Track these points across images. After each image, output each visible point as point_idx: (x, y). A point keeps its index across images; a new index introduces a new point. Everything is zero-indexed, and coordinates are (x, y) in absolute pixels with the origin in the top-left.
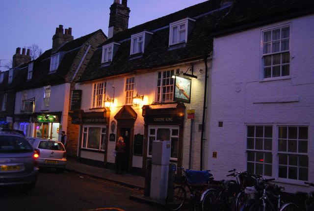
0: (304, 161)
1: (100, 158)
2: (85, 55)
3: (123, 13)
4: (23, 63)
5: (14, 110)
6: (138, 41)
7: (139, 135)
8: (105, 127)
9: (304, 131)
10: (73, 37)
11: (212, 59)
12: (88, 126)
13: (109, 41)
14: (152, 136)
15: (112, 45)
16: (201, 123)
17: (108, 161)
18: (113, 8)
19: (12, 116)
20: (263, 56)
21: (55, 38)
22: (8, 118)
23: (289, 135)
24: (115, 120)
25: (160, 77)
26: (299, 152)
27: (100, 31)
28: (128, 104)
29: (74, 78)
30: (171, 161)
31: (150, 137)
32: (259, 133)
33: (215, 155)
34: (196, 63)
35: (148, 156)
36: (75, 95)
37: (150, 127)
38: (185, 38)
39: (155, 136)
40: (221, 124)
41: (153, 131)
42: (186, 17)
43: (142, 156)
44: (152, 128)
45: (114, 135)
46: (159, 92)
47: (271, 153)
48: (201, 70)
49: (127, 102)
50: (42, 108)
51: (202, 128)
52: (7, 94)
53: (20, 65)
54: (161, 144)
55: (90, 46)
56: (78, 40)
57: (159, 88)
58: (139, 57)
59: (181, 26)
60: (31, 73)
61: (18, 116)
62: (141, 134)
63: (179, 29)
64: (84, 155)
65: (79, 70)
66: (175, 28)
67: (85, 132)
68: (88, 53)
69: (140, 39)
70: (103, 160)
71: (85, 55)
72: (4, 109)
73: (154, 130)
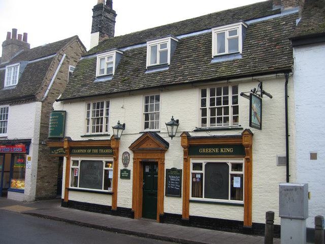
2: (60, 66)
3: (109, 16)
7: (173, 169)
10: (29, 45)
17: (119, 205)
18: (97, 9)
25: (89, 108)
29: (46, 95)
37: (193, 161)
40: (314, 156)
42: (239, 22)
45: (129, 172)
46: (88, 124)
49: (146, 126)
55: (65, 55)
56: (37, 49)
57: (88, 120)
62: (178, 168)
63: (106, 61)
64: (73, 197)
66: (102, 59)
71: (60, 66)
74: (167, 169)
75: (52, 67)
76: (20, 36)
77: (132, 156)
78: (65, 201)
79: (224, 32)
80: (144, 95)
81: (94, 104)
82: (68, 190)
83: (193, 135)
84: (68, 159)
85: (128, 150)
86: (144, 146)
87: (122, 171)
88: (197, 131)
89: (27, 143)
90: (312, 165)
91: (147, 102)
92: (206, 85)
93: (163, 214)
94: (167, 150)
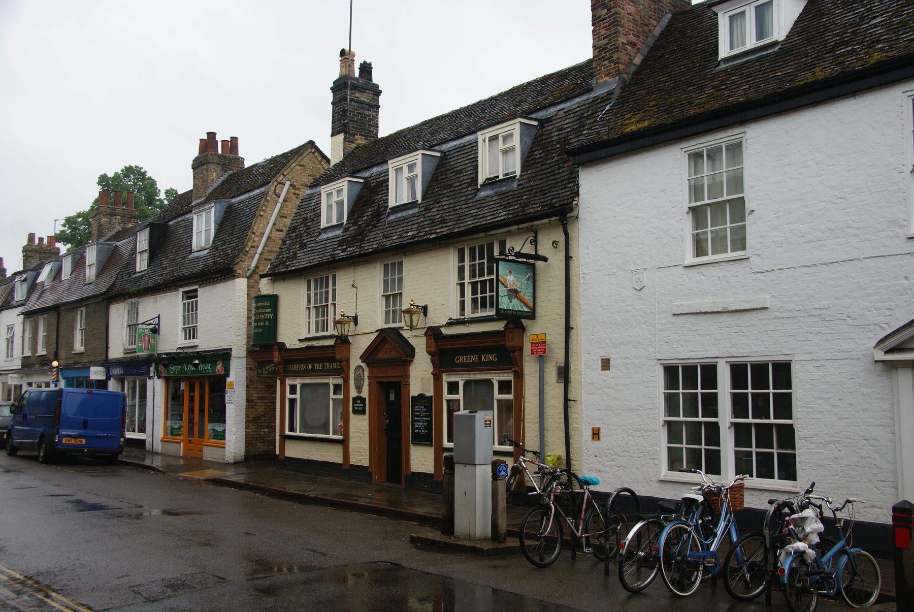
0: (787, 436)
1: (333, 455)
3: (364, 98)
4: (119, 228)
5: (107, 348)
6: (406, 173)
8: (340, 381)
9: (783, 371)
10: (242, 161)
11: (577, 217)
12: (298, 382)
13: (330, 177)
14: (293, 396)
15: (343, 184)
16: (562, 363)
17: (353, 461)
19: (102, 365)
20: (690, 208)
21: (198, 165)
22: (93, 369)
23: (670, 393)
24: (363, 365)
25: (461, 259)
26: (334, 434)
27: (311, 144)
28: (392, 325)
29: (253, 264)
30: (496, 453)
31: (449, 401)
32: (690, 382)
33: (596, 434)
34: (543, 227)
35: (446, 444)
36: (263, 307)
37: (446, 378)
38: (515, 165)
39: (460, 396)
40: (606, 364)
41: (453, 388)
43: (431, 445)
44: (453, 379)
45: (363, 400)
46: (462, 294)
47: (717, 423)
48: (554, 242)
50: (179, 343)
51: (564, 374)
52: (84, 309)
53: (113, 232)
54: (471, 420)
55: (288, 183)
57: (462, 286)
58: (411, 212)
59: (505, 139)
60: (146, 256)
61: (118, 363)
62: (428, 394)
63: (501, 145)
64: (294, 451)
65: (266, 245)
67: (293, 396)
68: (285, 200)
69: (411, 167)
70: (339, 460)
71: (279, 205)
72: (79, 347)
73: (457, 383)
74: (412, 397)
75: (264, 211)
76: (41, 239)
77: (366, 374)
78: (280, 457)
79: (402, 167)
80: (381, 262)
81: (472, 250)
82: (284, 438)
83: (445, 331)
84: (283, 383)
85: (359, 363)
86: (382, 355)
87: (355, 400)
88: (451, 323)
89: (224, 356)
90: (604, 381)
91: (386, 274)
92: (464, 241)
93: (283, 458)
94: (412, 361)
